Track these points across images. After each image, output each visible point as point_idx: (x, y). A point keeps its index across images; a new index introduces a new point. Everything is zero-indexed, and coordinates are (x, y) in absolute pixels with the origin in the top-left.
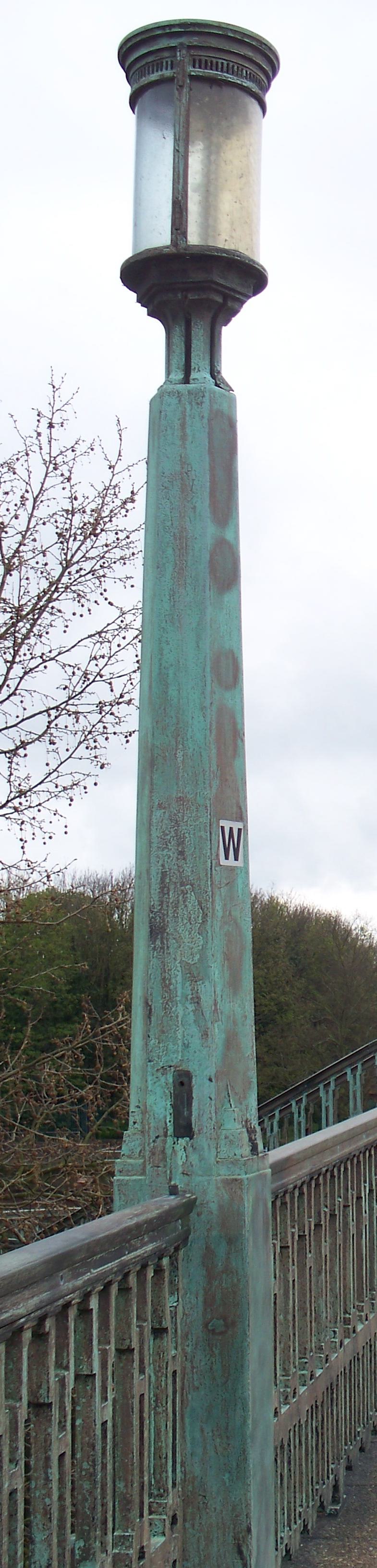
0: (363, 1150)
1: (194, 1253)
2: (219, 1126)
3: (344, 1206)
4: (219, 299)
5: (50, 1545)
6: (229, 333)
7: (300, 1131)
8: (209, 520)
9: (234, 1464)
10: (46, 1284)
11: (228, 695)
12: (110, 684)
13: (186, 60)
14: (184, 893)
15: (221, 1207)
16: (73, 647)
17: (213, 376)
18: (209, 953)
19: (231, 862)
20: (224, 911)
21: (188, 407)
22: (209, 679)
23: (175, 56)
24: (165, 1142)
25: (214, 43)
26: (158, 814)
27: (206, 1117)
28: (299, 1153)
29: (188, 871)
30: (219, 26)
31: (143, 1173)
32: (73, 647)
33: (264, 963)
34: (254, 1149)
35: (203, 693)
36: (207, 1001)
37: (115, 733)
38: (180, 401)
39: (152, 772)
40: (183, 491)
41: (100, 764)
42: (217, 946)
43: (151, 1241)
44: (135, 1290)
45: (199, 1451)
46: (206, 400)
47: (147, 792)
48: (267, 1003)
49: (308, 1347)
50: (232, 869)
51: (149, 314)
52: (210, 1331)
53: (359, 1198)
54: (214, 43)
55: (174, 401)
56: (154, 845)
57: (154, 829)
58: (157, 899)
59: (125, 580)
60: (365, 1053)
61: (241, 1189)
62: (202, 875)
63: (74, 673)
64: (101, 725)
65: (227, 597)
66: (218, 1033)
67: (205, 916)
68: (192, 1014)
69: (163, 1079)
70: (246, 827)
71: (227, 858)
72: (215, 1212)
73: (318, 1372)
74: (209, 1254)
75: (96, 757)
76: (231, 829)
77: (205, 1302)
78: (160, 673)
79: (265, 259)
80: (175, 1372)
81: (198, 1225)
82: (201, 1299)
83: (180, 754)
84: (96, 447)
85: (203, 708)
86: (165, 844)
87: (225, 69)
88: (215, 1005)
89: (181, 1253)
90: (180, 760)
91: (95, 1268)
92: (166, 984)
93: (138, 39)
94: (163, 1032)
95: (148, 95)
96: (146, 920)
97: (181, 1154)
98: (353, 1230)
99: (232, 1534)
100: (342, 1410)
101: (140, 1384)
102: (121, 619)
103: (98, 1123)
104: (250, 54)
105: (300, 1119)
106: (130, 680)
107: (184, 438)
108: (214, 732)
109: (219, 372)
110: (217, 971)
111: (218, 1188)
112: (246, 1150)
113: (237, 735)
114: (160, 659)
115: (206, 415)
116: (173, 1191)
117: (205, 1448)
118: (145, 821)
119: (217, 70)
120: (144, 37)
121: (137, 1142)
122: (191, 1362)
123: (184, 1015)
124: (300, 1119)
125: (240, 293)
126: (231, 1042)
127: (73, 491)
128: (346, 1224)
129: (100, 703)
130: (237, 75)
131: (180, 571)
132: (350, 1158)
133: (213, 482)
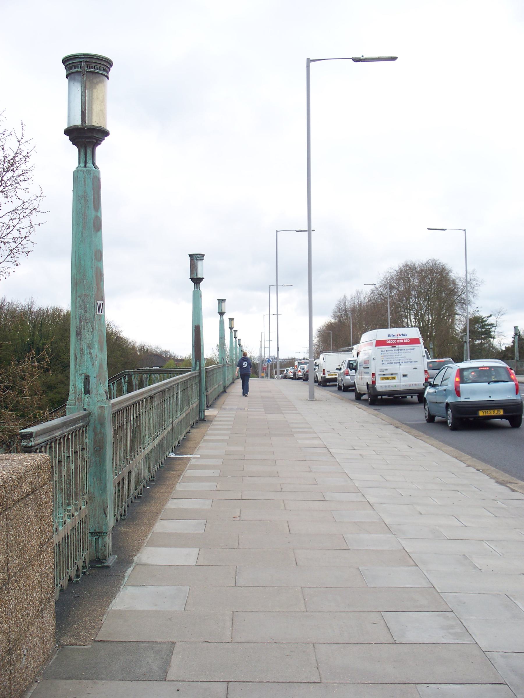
0: (132, 404)
1: (90, 428)
2: (97, 391)
3: (127, 422)
4: (95, 141)
5: (62, 498)
6: (98, 149)
7: (114, 396)
8: (93, 210)
9: (103, 489)
10: (61, 429)
11: (99, 263)
12: (20, 231)
13: (85, 66)
14: (87, 323)
15: (98, 415)
16: (4, 216)
17: (93, 165)
18: (94, 340)
19: (100, 313)
20: (98, 328)
21: (86, 175)
22: (93, 258)
23: (82, 64)
24: (81, 396)
25: (94, 61)
26: (78, 299)
27: (94, 388)
28: (115, 402)
29: (87, 315)
30: (95, 56)
31: (75, 405)
32: (4, 216)
33: (65, 340)
34: (107, 398)
35: (92, 263)
36: (94, 355)
37: (23, 252)
38: (83, 173)
39: (76, 286)
40: (85, 201)
41: (16, 264)
42: (96, 338)
43: (81, 422)
44: (78, 435)
45: (93, 485)
46: (92, 173)
47: (75, 292)
48: (66, 358)
49: (117, 464)
50: (100, 315)
51: (73, 144)
52: (95, 451)
53: (131, 420)
54: (94, 61)
55: (82, 173)
56: (77, 308)
57: (77, 303)
58: (78, 324)
59: (25, 190)
60: (118, 377)
61: (104, 409)
62: (92, 317)
63: (3, 226)
64: (17, 249)
65: (98, 233)
66: (97, 364)
67: (93, 329)
68: (89, 358)
69: (81, 377)
70: (104, 303)
71: (99, 312)
72: (97, 416)
73: (120, 473)
74: (95, 428)
75: (15, 261)
76: (100, 303)
77: (94, 442)
78: (79, 257)
79: (109, 128)
80: (86, 461)
81: (92, 420)
82: (93, 441)
83: (85, 281)
84: (13, 134)
85: (92, 267)
86: (81, 308)
87: (97, 69)
88: (96, 355)
89: (88, 427)
90: (85, 283)
91: (71, 427)
92: (81, 349)
93: (70, 58)
94: (81, 364)
95: (72, 76)
96: (75, 331)
97: (86, 399)
98: (129, 430)
99: (102, 508)
100: (126, 486)
101: (79, 462)
102: (23, 205)
103: (12, 405)
104: (104, 63)
105: (125, 388)
106: (29, 231)
107: (85, 184)
108: (95, 274)
109: (95, 163)
110: (96, 345)
111: (97, 409)
112: (105, 398)
113: (101, 275)
114: (79, 253)
115: (92, 178)
116: (85, 409)
117: (94, 484)
118: (74, 301)
119: (94, 69)
120: (71, 57)
121: (73, 396)
122: (90, 459)
123: (87, 359)
124: (125, 388)
125: (101, 139)
126: (101, 366)
127: (5, 154)
128: (127, 428)
129: (14, 238)
130: (100, 70)
131: (84, 226)
132: (128, 406)
133: (94, 199)
